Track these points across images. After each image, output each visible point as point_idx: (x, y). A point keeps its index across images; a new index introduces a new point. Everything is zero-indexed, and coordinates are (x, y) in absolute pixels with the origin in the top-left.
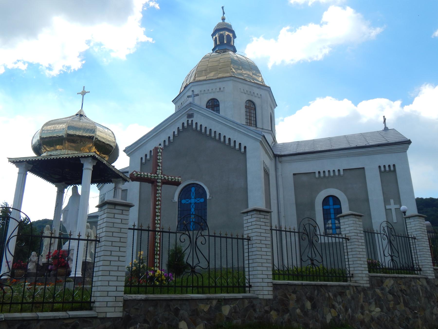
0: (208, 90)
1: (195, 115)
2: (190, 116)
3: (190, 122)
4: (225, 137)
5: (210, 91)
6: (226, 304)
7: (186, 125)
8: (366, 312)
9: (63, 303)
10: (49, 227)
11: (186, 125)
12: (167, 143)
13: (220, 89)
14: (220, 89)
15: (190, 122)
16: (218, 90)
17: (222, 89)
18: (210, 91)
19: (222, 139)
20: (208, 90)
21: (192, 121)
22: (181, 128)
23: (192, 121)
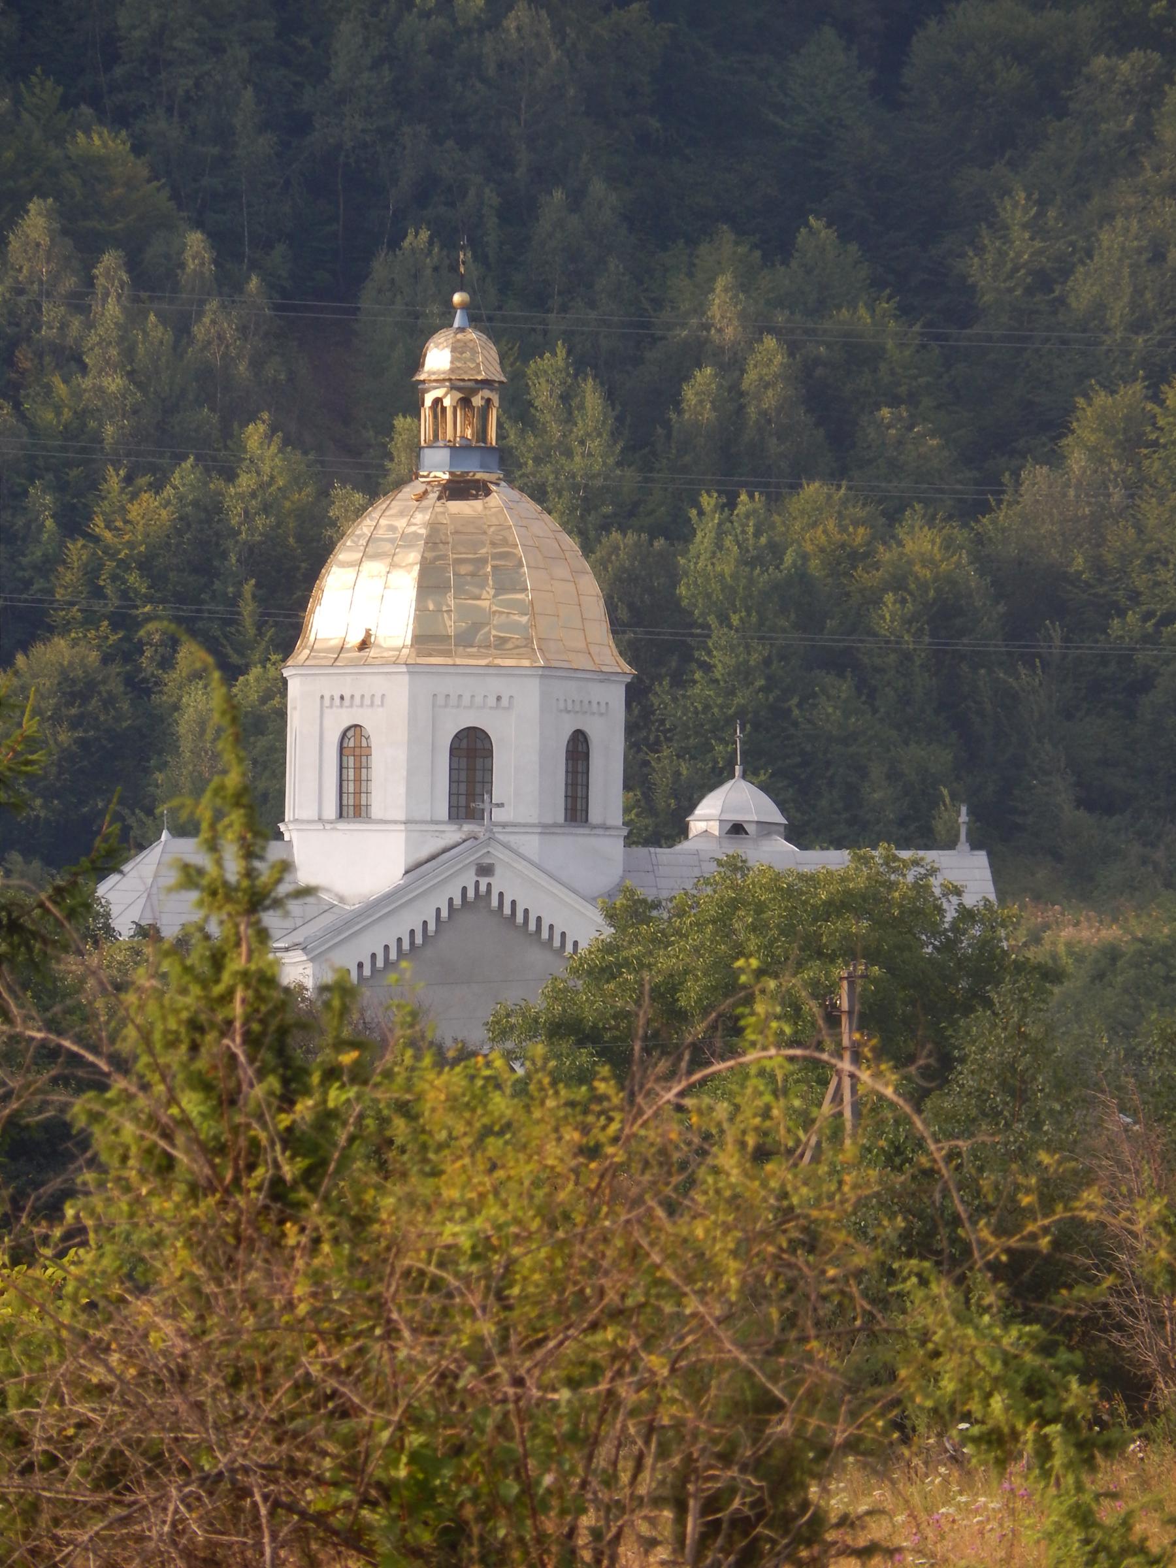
0: (460, 696)
1: (498, 870)
2: (485, 870)
3: (483, 888)
4: (539, 919)
5: (466, 700)
6: (440, 1195)
7: (471, 894)
8: (733, 1162)
9: (681, 1508)
10: (115, 1109)
11: (471, 894)
12: (419, 940)
13: (499, 698)
14: (499, 698)
15: (483, 888)
16: (492, 701)
17: (505, 702)
18: (466, 700)
19: (520, 918)
20: (460, 696)
21: (489, 885)
22: (457, 902)
23: (489, 885)
